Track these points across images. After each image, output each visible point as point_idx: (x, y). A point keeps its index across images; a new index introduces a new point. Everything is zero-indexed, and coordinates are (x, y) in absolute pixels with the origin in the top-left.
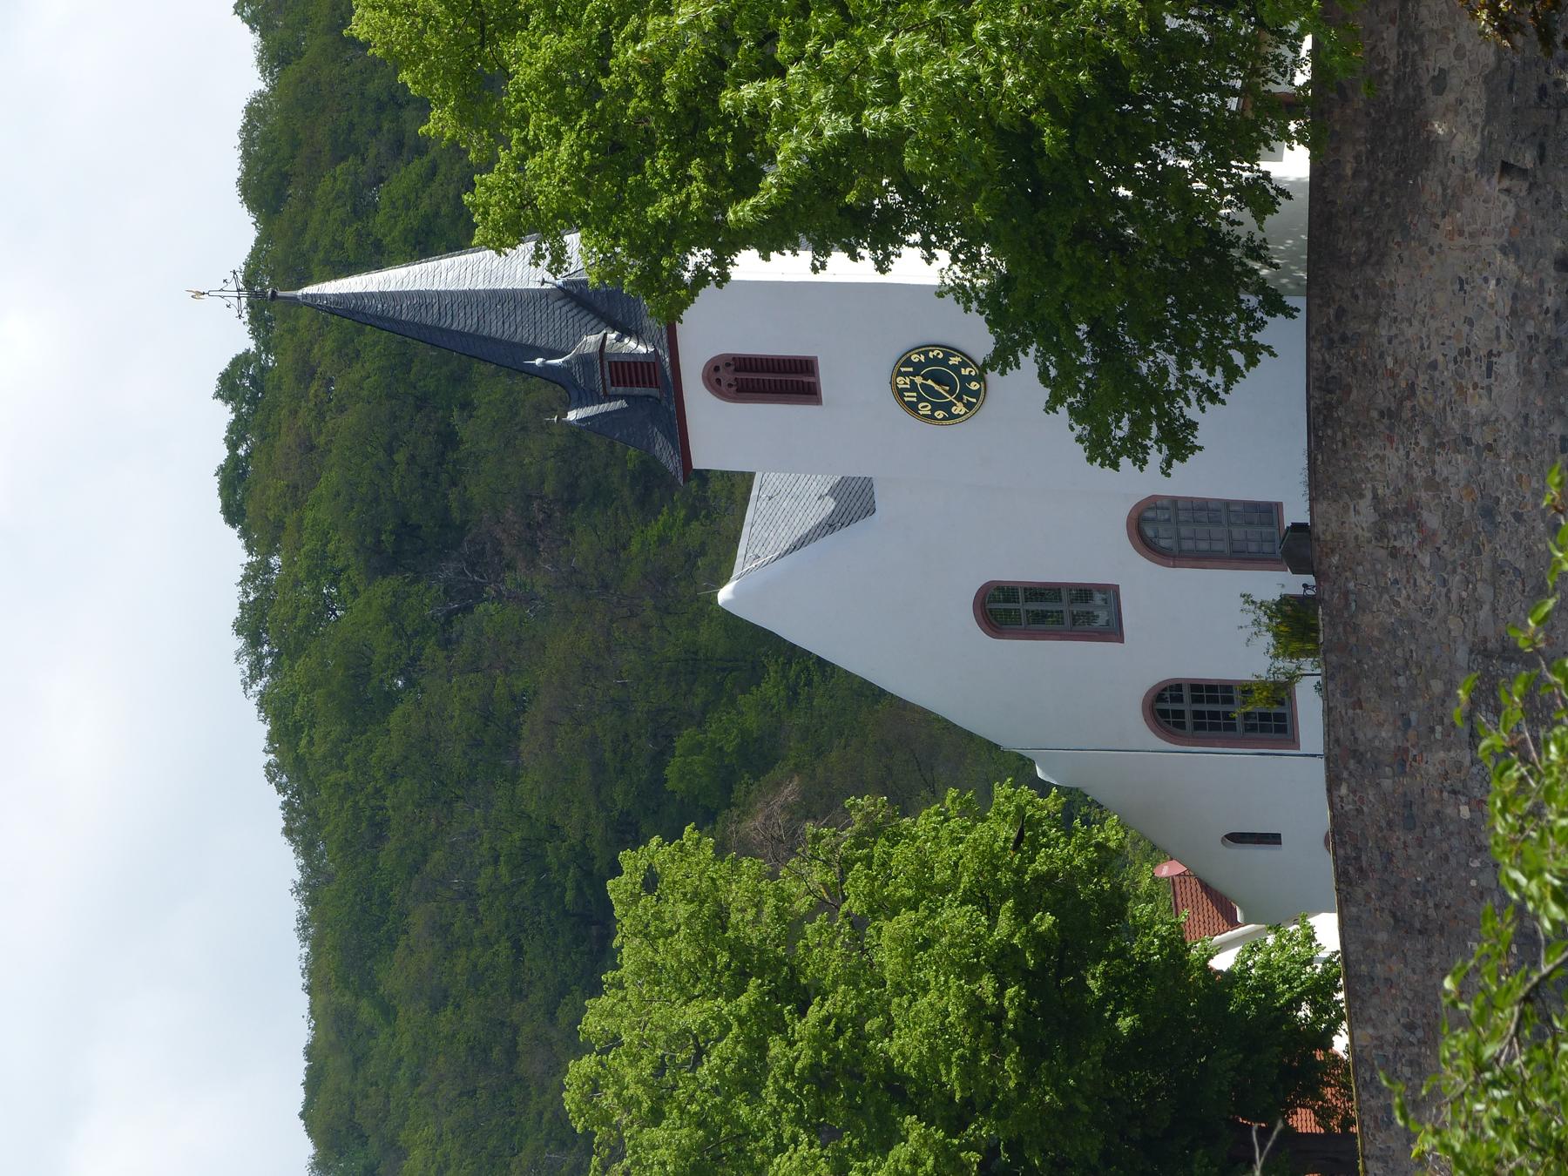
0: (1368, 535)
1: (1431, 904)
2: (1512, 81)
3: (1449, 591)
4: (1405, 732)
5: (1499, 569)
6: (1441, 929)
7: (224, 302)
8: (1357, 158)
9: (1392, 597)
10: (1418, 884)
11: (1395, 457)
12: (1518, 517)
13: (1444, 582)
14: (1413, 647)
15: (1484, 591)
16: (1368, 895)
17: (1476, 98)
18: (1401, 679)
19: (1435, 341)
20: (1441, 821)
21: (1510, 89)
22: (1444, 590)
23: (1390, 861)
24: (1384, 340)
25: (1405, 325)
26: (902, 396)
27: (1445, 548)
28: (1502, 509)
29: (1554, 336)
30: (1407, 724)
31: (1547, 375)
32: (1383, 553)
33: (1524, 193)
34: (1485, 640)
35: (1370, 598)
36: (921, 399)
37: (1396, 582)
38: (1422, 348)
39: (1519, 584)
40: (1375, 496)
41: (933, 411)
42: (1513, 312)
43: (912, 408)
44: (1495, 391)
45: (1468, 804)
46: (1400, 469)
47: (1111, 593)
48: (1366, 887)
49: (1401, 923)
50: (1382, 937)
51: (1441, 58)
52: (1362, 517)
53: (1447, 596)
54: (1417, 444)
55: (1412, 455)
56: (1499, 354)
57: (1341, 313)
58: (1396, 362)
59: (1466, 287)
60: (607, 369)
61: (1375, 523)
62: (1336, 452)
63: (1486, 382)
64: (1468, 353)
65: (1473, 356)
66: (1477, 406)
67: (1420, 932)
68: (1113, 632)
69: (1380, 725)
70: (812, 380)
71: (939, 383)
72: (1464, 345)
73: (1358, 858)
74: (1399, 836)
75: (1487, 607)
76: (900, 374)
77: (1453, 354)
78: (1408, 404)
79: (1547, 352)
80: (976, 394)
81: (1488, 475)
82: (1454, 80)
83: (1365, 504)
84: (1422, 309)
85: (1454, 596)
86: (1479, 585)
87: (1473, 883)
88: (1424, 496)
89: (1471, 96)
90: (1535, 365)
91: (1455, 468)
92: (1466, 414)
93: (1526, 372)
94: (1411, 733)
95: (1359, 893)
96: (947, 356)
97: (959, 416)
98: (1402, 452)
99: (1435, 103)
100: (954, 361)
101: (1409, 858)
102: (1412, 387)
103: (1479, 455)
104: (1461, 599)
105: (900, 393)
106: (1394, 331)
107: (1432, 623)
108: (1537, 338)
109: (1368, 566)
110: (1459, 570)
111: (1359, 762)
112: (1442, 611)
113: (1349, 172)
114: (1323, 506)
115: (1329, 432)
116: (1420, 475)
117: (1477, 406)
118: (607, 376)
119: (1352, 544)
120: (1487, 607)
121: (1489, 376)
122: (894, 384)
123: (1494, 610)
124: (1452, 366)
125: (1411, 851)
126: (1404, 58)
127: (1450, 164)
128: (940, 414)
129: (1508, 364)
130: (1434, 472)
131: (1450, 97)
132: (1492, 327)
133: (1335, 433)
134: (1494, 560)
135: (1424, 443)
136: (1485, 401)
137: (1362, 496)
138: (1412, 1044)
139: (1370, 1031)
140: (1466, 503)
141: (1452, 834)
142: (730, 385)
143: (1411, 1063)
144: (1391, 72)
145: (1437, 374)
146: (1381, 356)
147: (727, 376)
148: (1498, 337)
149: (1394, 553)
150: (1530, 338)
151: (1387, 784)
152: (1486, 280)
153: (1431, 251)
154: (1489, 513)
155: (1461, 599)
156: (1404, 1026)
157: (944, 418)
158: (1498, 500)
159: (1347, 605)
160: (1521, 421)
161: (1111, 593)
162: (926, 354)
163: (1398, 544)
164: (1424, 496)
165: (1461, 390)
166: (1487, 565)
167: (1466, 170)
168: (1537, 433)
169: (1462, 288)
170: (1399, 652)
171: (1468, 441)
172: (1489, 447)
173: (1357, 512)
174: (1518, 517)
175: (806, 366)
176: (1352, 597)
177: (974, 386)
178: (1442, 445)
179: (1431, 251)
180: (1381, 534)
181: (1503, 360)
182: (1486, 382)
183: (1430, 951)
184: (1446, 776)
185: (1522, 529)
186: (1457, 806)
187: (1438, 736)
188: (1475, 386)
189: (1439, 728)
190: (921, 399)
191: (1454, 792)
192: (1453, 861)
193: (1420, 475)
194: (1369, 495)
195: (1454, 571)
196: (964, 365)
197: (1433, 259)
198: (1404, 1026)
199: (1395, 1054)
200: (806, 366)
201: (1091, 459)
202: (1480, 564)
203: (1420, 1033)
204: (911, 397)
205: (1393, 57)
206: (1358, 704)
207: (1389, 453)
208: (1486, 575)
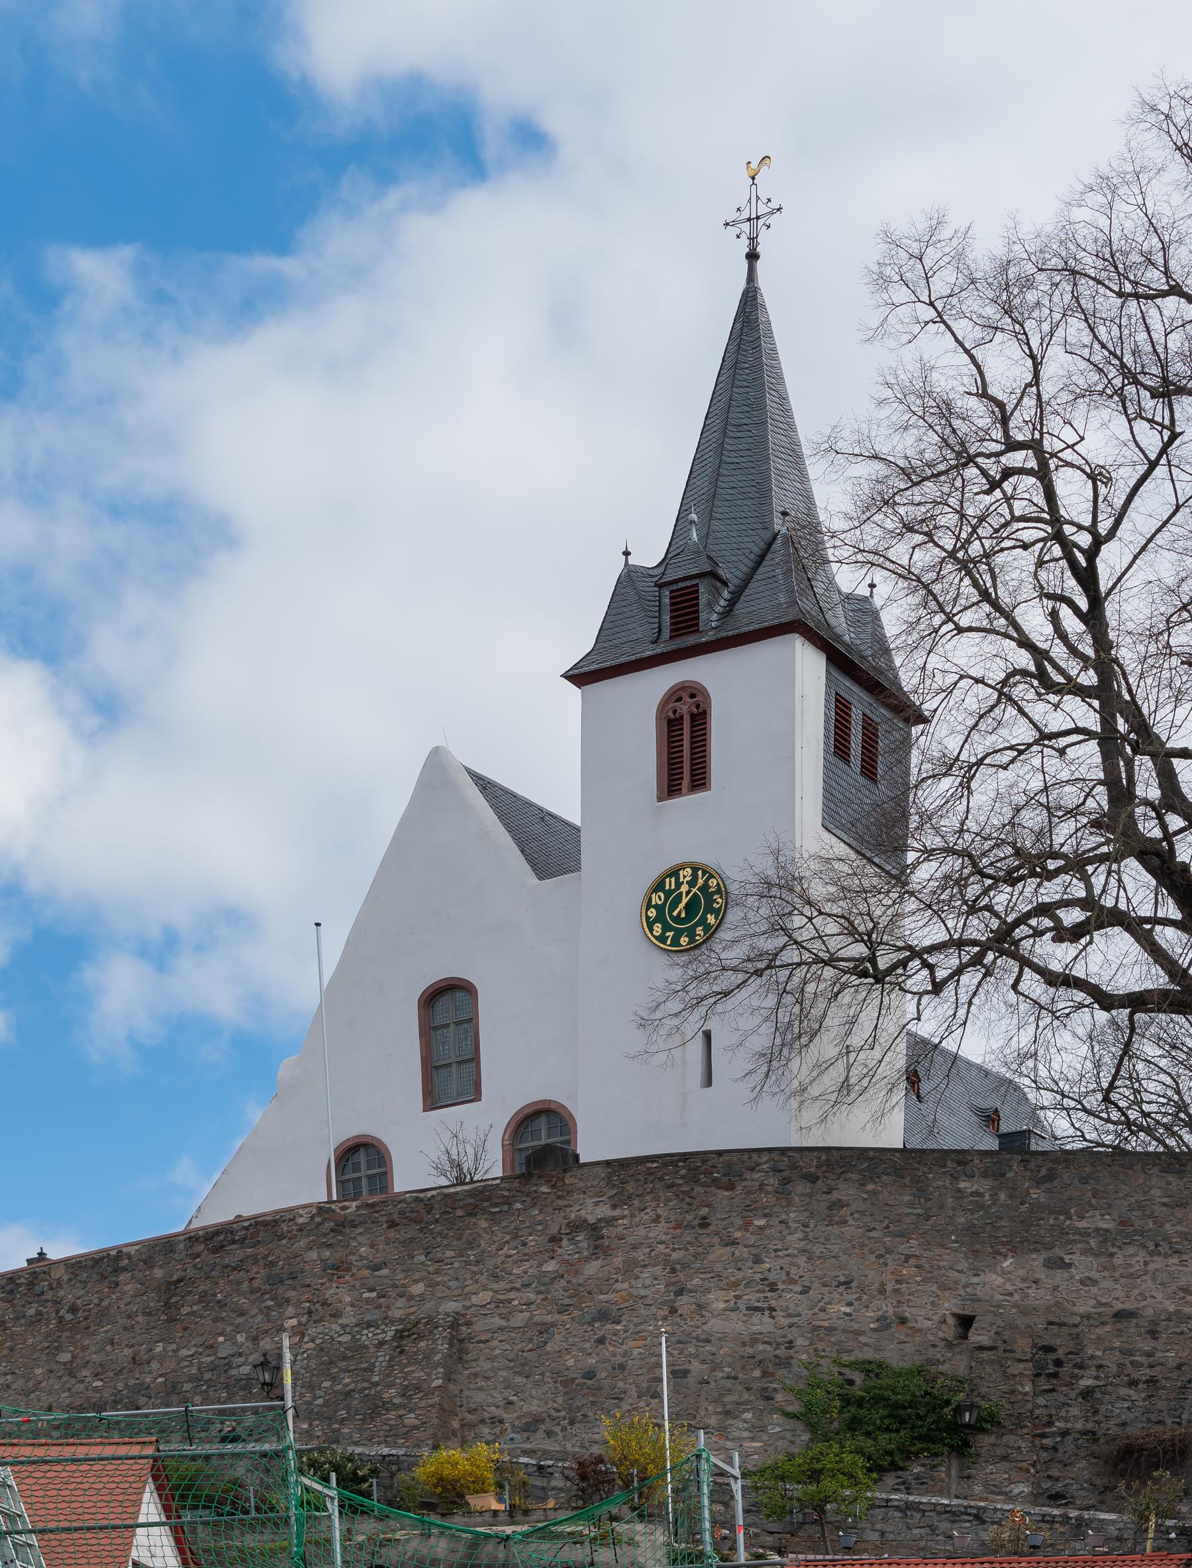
0: (573, 1216)
1: (195, 1308)
2: (1060, 1325)
3: (517, 1290)
4: (367, 1268)
5: (545, 1329)
6: (171, 1320)
7: (743, 203)
8: (976, 1193)
9: (507, 1242)
10: (215, 1295)
11: (660, 1231)
12: (601, 1341)
13: (527, 1285)
14: (456, 1265)
15: (520, 1319)
16: (198, 1255)
17: (1039, 1297)
18: (423, 1258)
19: (784, 1262)
20: (280, 1306)
21: (1051, 1323)
22: (518, 1285)
23: (234, 1269)
24: (784, 1217)
25: (799, 1235)
26: (670, 876)
27: (563, 1283)
28: (609, 1326)
29: (793, 1362)
30: (376, 1268)
31: (753, 1357)
32: (554, 1230)
33: (941, 1334)
34: (468, 1324)
35: (504, 1224)
36: (668, 894)
37: (524, 1244)
38: (776, 1251)
39: (530, 1346)
40: (616, 1219)
41: (656, 907)
42: (816, 1328)
43: (659, 886)
44: (733, 1315)
45: (300, 1323)
46: (647, 1237)
47: (474, 1093)
48: (205, 1253)
49: (171, 1286)
50: (158, 1273)
51: (1083, 1265)
52: (593, 1210)
53: (512, 1289)
54: (674, 1250)
55: (662, 1247)
56: (773, 1317)
57: (812, 1179)
58: (761, 1228)
59: (842, 1288)
60: (689, 583)
61: (585, 1221)
62: (661, 1179)
63: (742, 1305)
64: (772, 1290)
65: (769, 1294)
66: (718, 1300)
67: (166, 1303)
68: (432, 1100)
69: (372, 1246)
70: (684, 790)
71: (686, 907)
72: (781, 1286)
73: (234, 1242)
74: (260, 1273)
75: (503, 1323)
76: (695, 870)
77: (772, 1277)
78: (716, 1240)
79: (776, 1356)
80: (675, 942)
81: (644, 1312)
82: (1059, 1276)
83: (604, 1211)
84: (818, 1250)
85: (512, 1295)
86: (527, 1314)
87: (221, 1339)
88: (618, 1261)
89: (1042, 1292)
90: (761, 1347)
91: (650, 1283)
92: (708, 1291)
93: (754, 1340)
94: (367, 1272)
95: (200, 1248)
96: (716, 912)
97: (651, 931)
98: (664, 1238)
99: (1036, 1260)
100: (711, 919)
101: (239, 1283)
102: (734, 1243)
103: (664, 1303)
104: (510, 1301)
105: (674, 873)
106: (793, 1225)
107: (483, 1279)
108: (791, 1348)
109: (539, 1218)
110: (541, 1297)
111: (332, 1230)
112: (495, 1286)
113: (962, 1185)
114: (602, 1172)
115: (683, 1172)
116: (641, 1255)
117: (718, 1300)
118: (681, 585)
119: (561, 1203)
120: (503, 1323)
121: (748, 1309)
122: (683, 867)
123: (501, 1329)
124: (757, 1277)
125: (245, 1285)
126: (1085, 1234)
127: (972, 1273)
128: (653, 913)
129: (762, 1324)
130: (645, 1266)
131: (1041, 1275)
132: (800, 1309)
133: (682, 1177)
134: (553, 1325)
135: (675, 1256)
136: (722, 1305)
137: (614, 1207)
138: (57, 1312)
139: (65, 1278)
140: (610, 1296)
141: (268, 1315)
142: (675, 712)
143: (39, 1313)
144: (1068, 1222)
145: (750, 1264)
146: (765, 1216)
147: (685, 708)
148: (789, 1316)
149: (555, 1240)
150: (791, 1342)
151: (313, 1255)
152: (849, 1304)
153: (880, 1256)
154: (603, 1316)
155: (510, 1301)
156: (74, 1304)
157: (648, 918)
158: (618, 1323)
159: (496, 1205)
160: (702, 1337)
161: (474, 1093)
162: (719, 891)
163: (565, 1242)
164: (618, 1261)
165: (735, 1285)
166: (549, 1319)
167: (965, 1287)
168: (692, 1350)
169: (840, 1284)
170: (449, 1253)
171: (680, 1292)
172: (673, 1311)
173: (597, 1204)
174: (601, 1341)
175: (700, 781)
176: (505, 1208)
177: (684, 940)
178: (673, 1271)
179: (880, 1256)
180: (576, 1226)
181: (766, 1318)
182: (742, 1307)
183: (149, 1314)
184: (325, 1304)
185: (587, 1345)
186: (297, 1316)
187: (366, 1295)
188: (737, 1297)
189: (374, 1295)
190: (668, 894)
191: (310, 1312)
192: (240, 1320)
193: (641, 1255)
194: (617, 1213)
195: (538, 1293)
196: (707, 927)
197: (873, 1258)
198: (74, 1304)
199: (47, 1301)
200: (700, 781)
201: (890, 239)
202: (549, 1313)
203: (69, 1317)
204: (670, 883)
205: (1083, 1224)
206: (392, 1224)
207: (662, 1226)
208: (537, 1319)
